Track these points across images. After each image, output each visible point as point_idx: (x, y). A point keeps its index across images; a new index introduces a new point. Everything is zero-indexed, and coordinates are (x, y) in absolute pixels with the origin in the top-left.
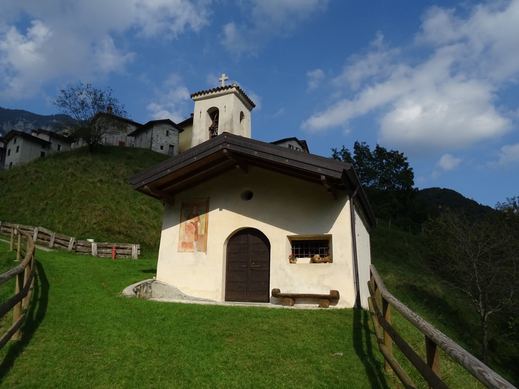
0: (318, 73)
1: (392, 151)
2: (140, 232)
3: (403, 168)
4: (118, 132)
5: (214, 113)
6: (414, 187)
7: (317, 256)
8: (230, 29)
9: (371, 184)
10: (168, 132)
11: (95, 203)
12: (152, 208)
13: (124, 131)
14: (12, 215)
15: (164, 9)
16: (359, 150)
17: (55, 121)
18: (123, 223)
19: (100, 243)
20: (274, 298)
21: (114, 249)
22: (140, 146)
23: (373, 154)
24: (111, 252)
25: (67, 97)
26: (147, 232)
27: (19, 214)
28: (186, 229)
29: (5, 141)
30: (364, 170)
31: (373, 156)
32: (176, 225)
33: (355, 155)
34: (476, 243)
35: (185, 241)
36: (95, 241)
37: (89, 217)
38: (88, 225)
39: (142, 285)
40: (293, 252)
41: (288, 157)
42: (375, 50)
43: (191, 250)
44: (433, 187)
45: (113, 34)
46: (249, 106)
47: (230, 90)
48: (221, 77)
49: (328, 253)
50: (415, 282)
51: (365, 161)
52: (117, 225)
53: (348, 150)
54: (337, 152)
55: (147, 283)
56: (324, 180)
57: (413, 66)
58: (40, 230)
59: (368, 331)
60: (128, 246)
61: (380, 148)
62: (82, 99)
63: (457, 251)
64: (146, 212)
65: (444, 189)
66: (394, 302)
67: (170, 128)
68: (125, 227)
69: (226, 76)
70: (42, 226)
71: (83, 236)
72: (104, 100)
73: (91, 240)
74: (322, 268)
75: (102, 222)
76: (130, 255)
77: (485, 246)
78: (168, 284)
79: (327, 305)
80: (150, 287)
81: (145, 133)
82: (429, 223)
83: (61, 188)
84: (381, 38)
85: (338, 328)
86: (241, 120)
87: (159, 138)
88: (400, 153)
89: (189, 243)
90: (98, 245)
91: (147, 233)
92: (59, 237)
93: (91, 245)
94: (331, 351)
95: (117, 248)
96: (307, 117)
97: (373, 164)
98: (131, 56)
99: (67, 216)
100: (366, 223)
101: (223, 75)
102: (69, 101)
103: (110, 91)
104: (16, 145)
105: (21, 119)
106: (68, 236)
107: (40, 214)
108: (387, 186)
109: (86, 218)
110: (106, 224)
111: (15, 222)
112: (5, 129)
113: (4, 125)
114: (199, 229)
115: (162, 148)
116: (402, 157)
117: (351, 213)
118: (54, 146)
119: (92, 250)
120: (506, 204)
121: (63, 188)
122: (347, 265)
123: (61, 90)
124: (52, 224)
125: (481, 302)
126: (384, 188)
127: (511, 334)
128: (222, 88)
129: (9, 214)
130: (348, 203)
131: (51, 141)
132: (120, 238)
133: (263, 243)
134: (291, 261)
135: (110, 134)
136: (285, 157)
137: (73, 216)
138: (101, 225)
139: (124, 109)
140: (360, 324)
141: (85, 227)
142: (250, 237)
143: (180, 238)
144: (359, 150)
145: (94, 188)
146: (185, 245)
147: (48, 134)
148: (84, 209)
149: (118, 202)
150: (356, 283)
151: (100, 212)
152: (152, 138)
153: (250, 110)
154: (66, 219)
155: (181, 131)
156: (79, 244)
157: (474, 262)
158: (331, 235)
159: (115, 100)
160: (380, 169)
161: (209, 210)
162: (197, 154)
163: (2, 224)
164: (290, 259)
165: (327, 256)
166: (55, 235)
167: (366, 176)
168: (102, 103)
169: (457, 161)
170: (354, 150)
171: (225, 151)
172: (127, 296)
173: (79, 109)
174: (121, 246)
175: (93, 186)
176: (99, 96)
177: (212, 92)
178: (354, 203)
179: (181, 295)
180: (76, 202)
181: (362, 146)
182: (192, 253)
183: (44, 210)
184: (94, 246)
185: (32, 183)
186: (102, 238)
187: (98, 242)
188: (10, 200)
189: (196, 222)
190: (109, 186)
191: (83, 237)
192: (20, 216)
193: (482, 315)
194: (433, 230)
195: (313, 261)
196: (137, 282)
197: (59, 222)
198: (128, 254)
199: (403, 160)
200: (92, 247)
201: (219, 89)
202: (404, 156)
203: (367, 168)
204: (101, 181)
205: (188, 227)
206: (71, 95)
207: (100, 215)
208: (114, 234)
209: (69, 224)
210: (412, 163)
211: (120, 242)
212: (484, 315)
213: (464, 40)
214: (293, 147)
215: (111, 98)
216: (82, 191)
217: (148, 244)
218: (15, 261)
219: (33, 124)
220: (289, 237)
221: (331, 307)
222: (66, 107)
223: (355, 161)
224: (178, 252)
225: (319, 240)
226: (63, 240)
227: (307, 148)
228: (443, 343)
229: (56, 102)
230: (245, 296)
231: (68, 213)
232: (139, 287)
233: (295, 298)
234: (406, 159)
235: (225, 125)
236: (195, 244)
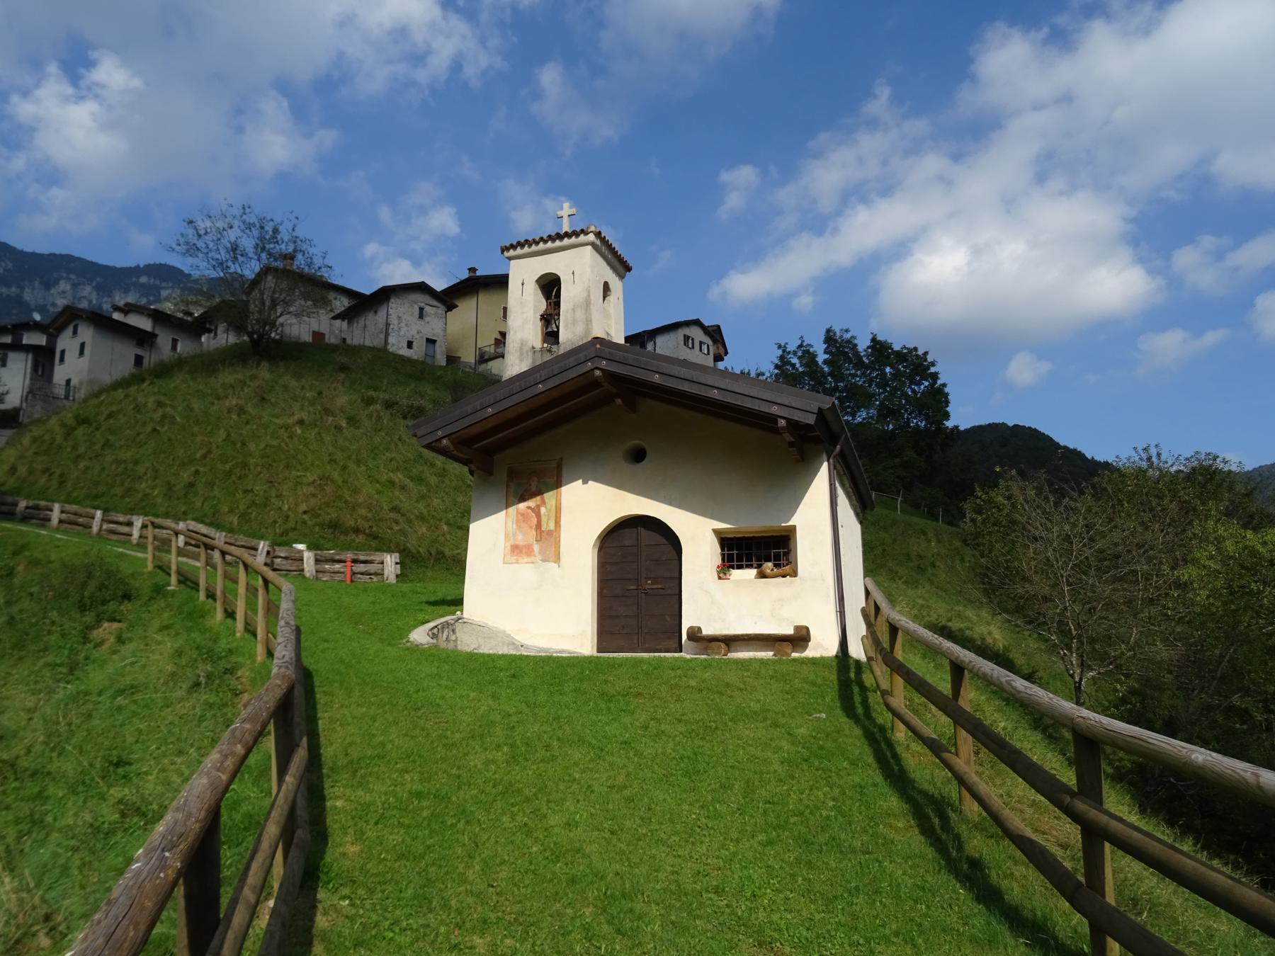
0: (745, 175)
1: (905, 348)
2: (397, 528)
3: (927, 383)
4: (314, 313)
5: (550, 286)
6: (949, 424)
7: (768, 566)
8: (550, 77)
9: (861, 420)
10: (421, 309)
11: (298, 471)
12: (412, 478)
13: (329, 309)
14: (123, 497)
15: (401, 32)
16: (836, 347)
17: (144, 279)
18: (363, 512)
19: (319, 552)
20: (691, 642)
21: (349, 564)
22: (362, 340)
23: (864, 356)
24: (342, 570)
25: (200, 236)
26: (411, 527)
27: (140, 496)
28: (518, 521)
29: (51, 330)
30: (845, 389)
31: (864, 359)
32: (496, 513)
33: (827, 356)
34: (1068, 538)
35: (517, 543)
36: (309, 548)
37: (291, 500)
38: (292, 515)
39: (439, 627)
40: (723, 560)
41: (716, 385)
42: (873, 124)
43: (529, 559)
44: (991, 422)
45: (283, 86)
46: (621, 269)
47: (582, 238)
48: (562, 209)
49: (787, 560)
50: (950, 620)
51: (849, 369)
52: (351, 515)
53: (812, 346)
54: (788, 350)
55: (447, 623)
56: (783, 428)
57: (957, 158)
58: (191, 528)
59: (863, 689)
60: (377, 557)
61: (880, 343)
62: (233, 239)
63: (1032, 555)
64: (403, 488)
65: (1016, 426)
66: (907, 625)
67: (427, 302)
68: (366, 519)
69: (571, 207)
70: (194, 519)
71: (284, 539)
72: (283, 242)
73: (301, 547)
74: (777, 587)
75: (320, 509)
76: (380, 574)
77: (1085, 545)
78: (487, 624)
79: (790, 651)
80: (454, 631)
81: (372, 312)
82: (978, 501)
83: (220, 440)
84: (884, 93)
85: (813, 684)
86: (604, 298)
87: (403, 325)
88: (920, 352)
89: (525, 546)
90: (316, 555)
91: (409, 529)
92: (232, 541)
93: (302, 557)
94: (807, 713)
95: (355, 561)
96: (720, 274)
97: (864, 375)
98: (328, 137)
99: (245, 498)
100: (855, 502)
101: (566, 205)
102: (206, 243)
103: (295, 221)
104: (78, 341)
105: (64, 275)
106: (253, 538)
107: (185, 495)
108: (893, 424)
109: (285, 502)
110: (328, 514)
111: (131, 511)
112: (28, 299)
113: (27, 290)
114: (544, 519)
115: (410, 345)
116: (926, 360)
117: (831, 485)
118: (164, 339)
119: (305, 565)
120: (1132, 460)
121: (224, 440)
122: (823, 580)
123: (187, 220)
124: (214, 515)
125: (1074, 655)
126: (888, 426)
127: (1123, 708)
128: (567, 235)
129: (116, 495)
130: (825, 467)
131: (157, 332)
132: (357, 541)
133: (666, 542)
134: (721, 575)
135: (297, 315)
136: (711, 384)
137: (257, 498)
138: (318, 516)
139: (326, 262)
140: (849, 678)
141: (287, 520)
142: (647, 536)
143: (507, 536)
144: (836, 347)
145: (291, 437)
146: (516, 550)
147: (149, 316)
148: (279, 483)
149: (344, 468)
150: (840, 612)
151: (312, 489)
152: (388, 325)
153: (621, 277)
154: (245, 504)
155: (451, 307)
156: (277, 553)
157: (1062, 576)
158: (795, 527)
159: (307, 242)
160: (878, 386)
161: (563, 482)
162: (543, 379)
163: (103, 516)
164: (719, 573)
165: (787, 565)
166: (225, 537)
167: (850, 402)
168: (278, 247)
169: (1045, 367)
170: (825, 346)
171: (598, 373)
172: (422, 644)
173: (227, 261)
174: (362, 558)
175: (286, 434)
176: (271, 233)
177: (546, 242)
178: (835, 468)
179: (513, 644)
180: (259, 469)
181: (841, 337)
182: (531, 565)
183: (191, 485)
184: (309, 559)
185: (154, 430)
186: (322, 541)
187: (316, 550)
188: (114, 467)
189: (538, 507)
190: (319, 433)
191: (283, 540)
192: (142, 500)
193: (1077, 679)
194: (984, 516)
195: (762, 575)
196: (428, 621)
197: (231, 511)
198: (376, 574)
199: (928, 368)
200: (305, 559)
201: (560, 237)
202: (930, 359)
203: (851, 384)
204: (301, 422)
205: (523, 517)
206: (209, 230)
207: (314, 495)
208: (346, 533)
209: (251, 513)
210: (947, 374)
211: (359, 548)
212: (1081, 679)
213: (1066, 98)
214: (693, 339)
215: (297, 237)
216: (267, 446)
217: (414, 551)
218: (169, 588)
219: (93, 287)
220: (716, 532)
221: (795, 655)
222: (197, 257)
223: (826, 369)
224: (504, 563)
225: (763, 537)
226: (243, 546)
227: (723, 341)
228: (970, 662)
229: (174, 246)
230: (636, 641)
231: (246, 491)
232: (435, 631)
233: (730, 641)
234: (933, 364)
235: (574, 310)
236: (536, 548)
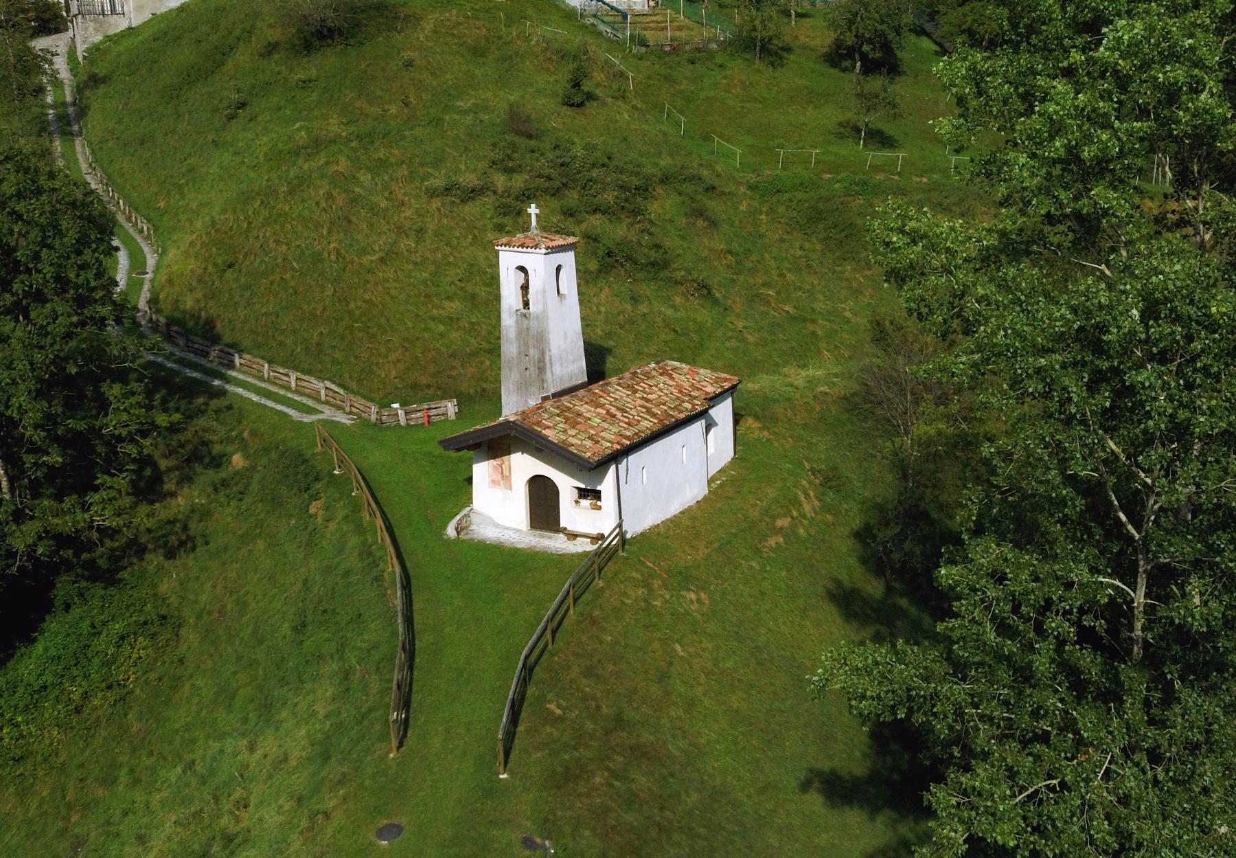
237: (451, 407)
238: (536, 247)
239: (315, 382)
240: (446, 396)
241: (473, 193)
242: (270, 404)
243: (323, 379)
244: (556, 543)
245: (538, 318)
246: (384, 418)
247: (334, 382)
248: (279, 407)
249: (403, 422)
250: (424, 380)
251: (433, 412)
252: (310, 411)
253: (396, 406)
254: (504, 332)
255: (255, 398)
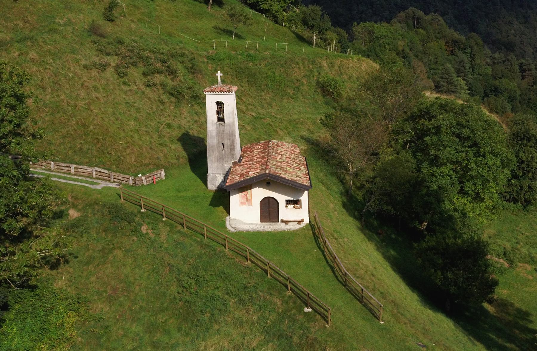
5: (220, 104)
114: (248, 197)
143: (239, 200)
237: (163, 173)
238: (229, 91)
239: (88, 168)
240: (158, 167)
241: (103, 67)
242: (66, 181)
243: (94, 167)
244: (279, 226)
245: (229, 125)
246: (137, 182)
247: (100, 167)
248: (79, 183)
249: (145, 184)
250: (147, 161)
251: (155, 177)
252: (95, 184)
253: (140, 175)
254: (209, 133)
255: (61, 180)
